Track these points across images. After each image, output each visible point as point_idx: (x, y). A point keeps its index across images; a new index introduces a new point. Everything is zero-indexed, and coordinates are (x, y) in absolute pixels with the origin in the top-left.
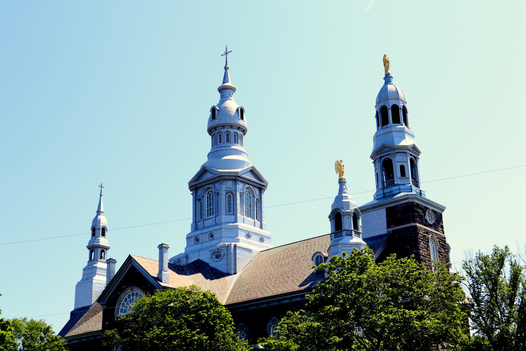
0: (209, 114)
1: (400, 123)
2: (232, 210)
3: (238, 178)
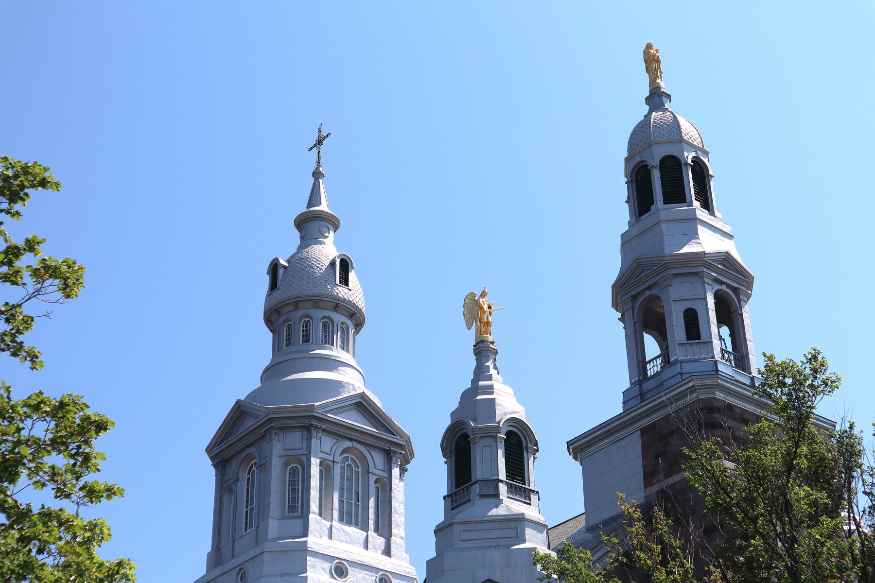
0: (266, 280)
1: (685, 202)
2: (297, 508)
3: (314, 423)
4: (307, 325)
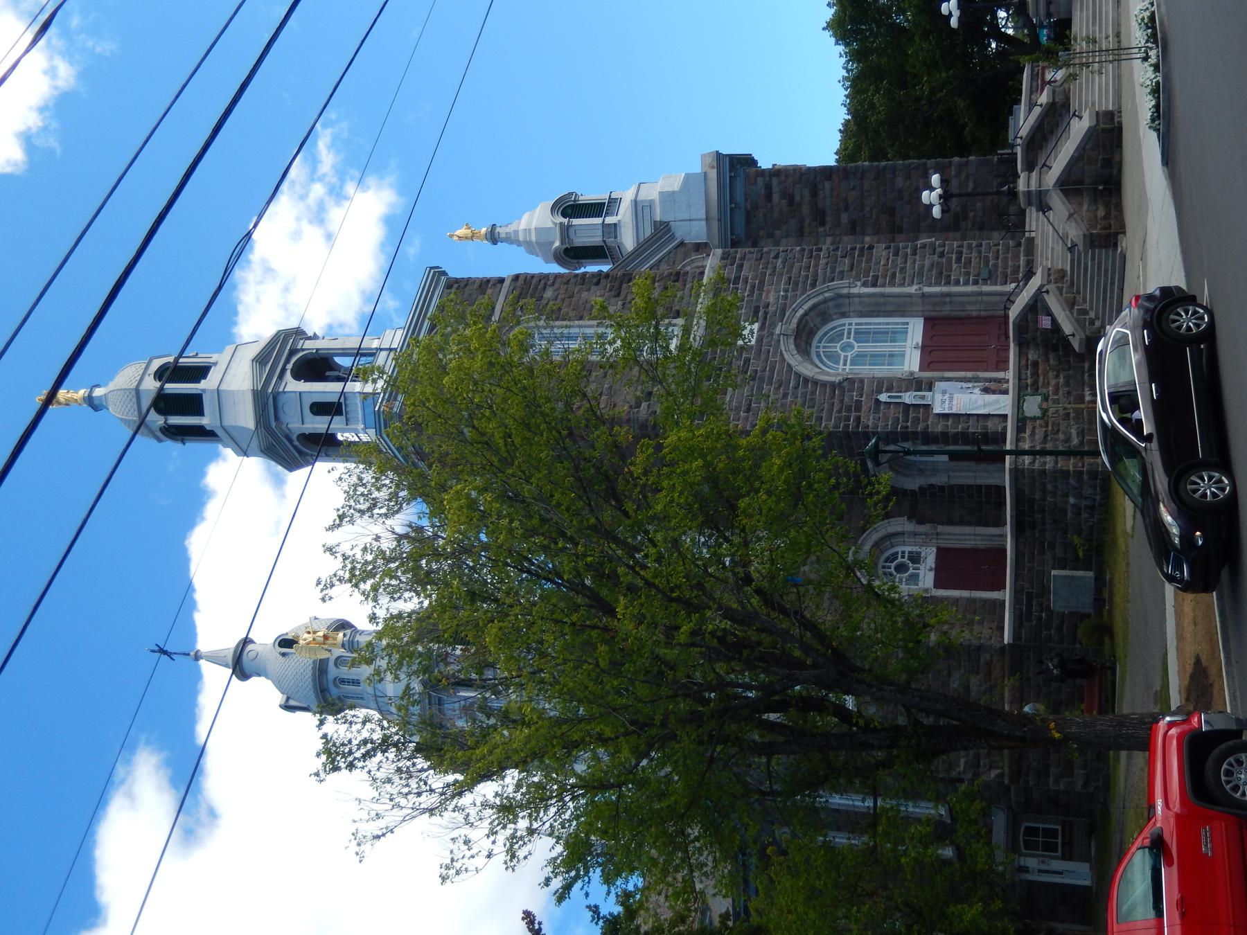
4: (343, 681)
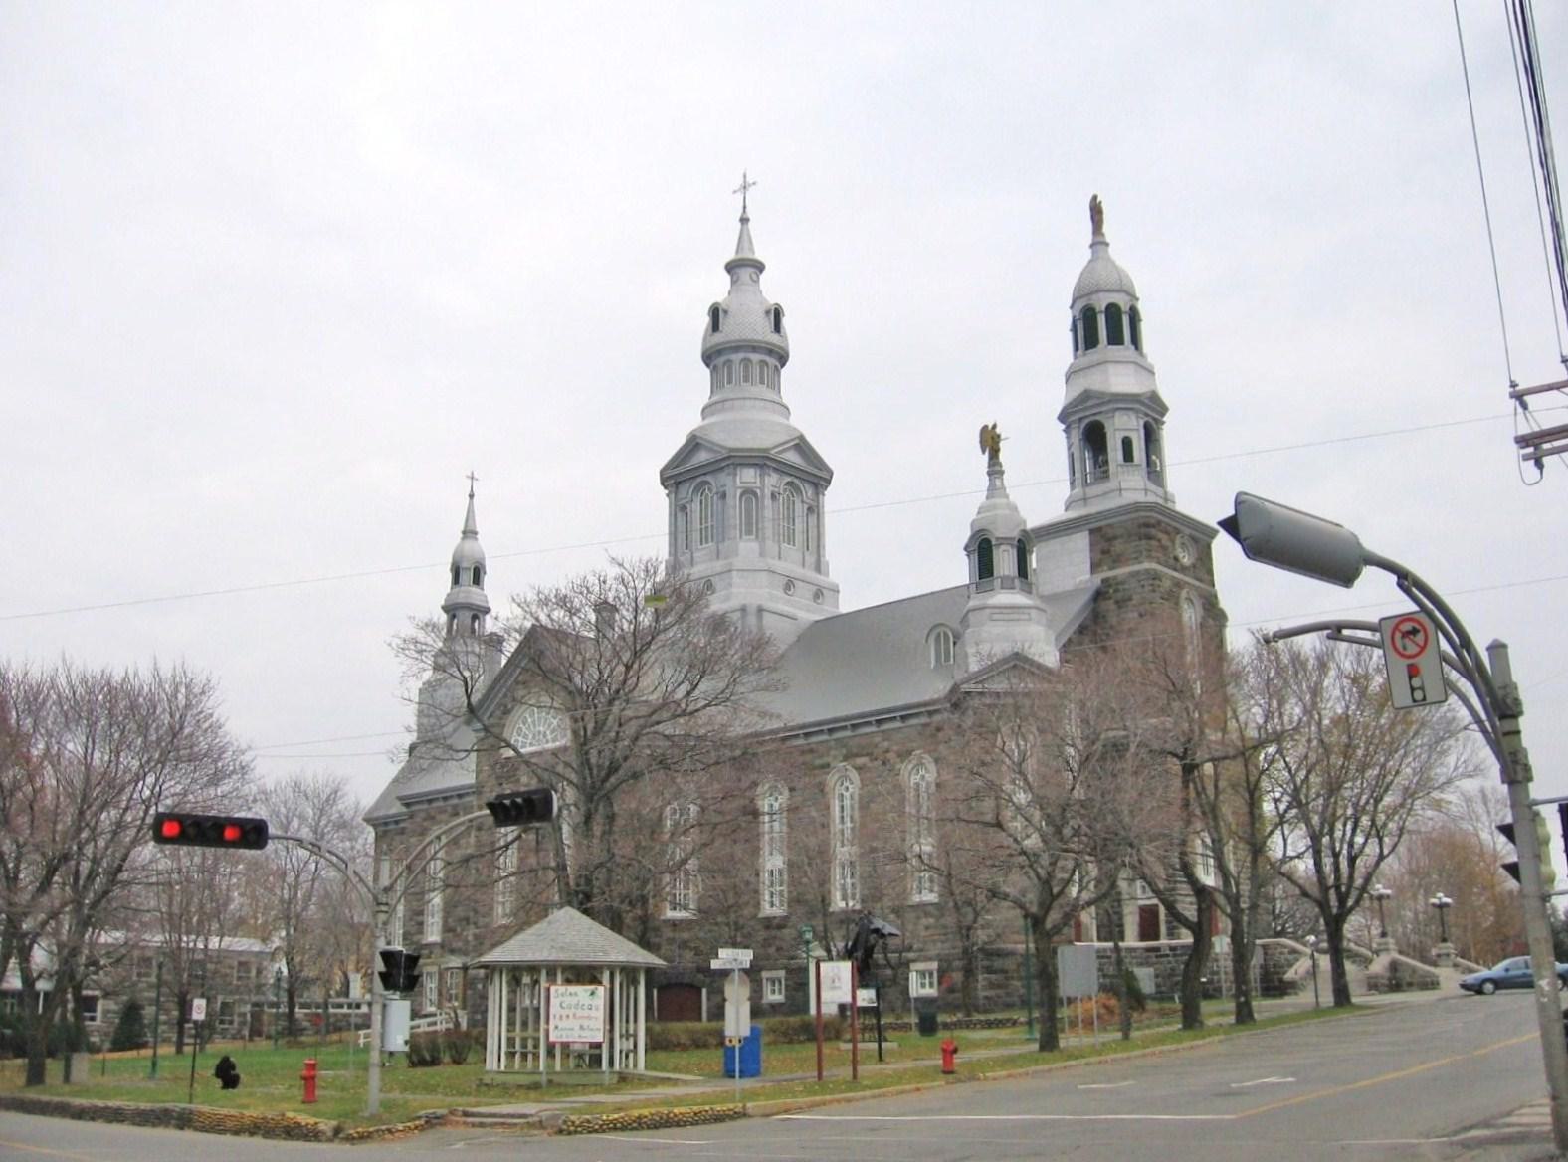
3: (768, 462)
